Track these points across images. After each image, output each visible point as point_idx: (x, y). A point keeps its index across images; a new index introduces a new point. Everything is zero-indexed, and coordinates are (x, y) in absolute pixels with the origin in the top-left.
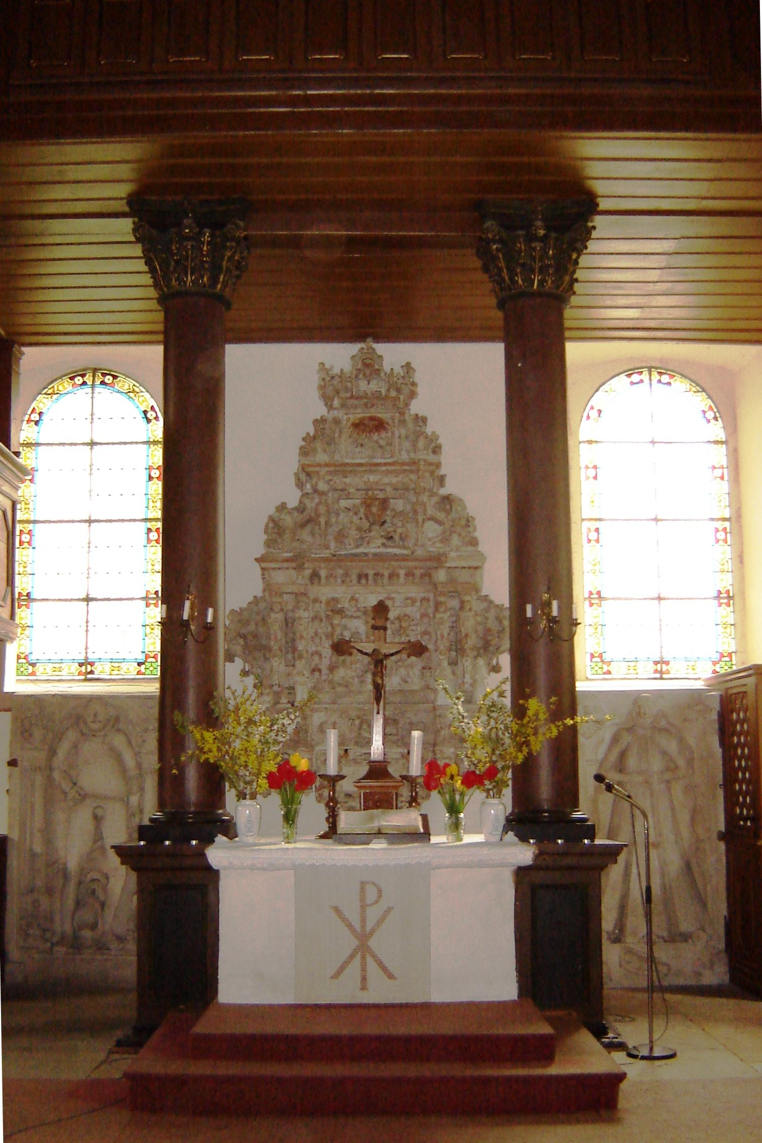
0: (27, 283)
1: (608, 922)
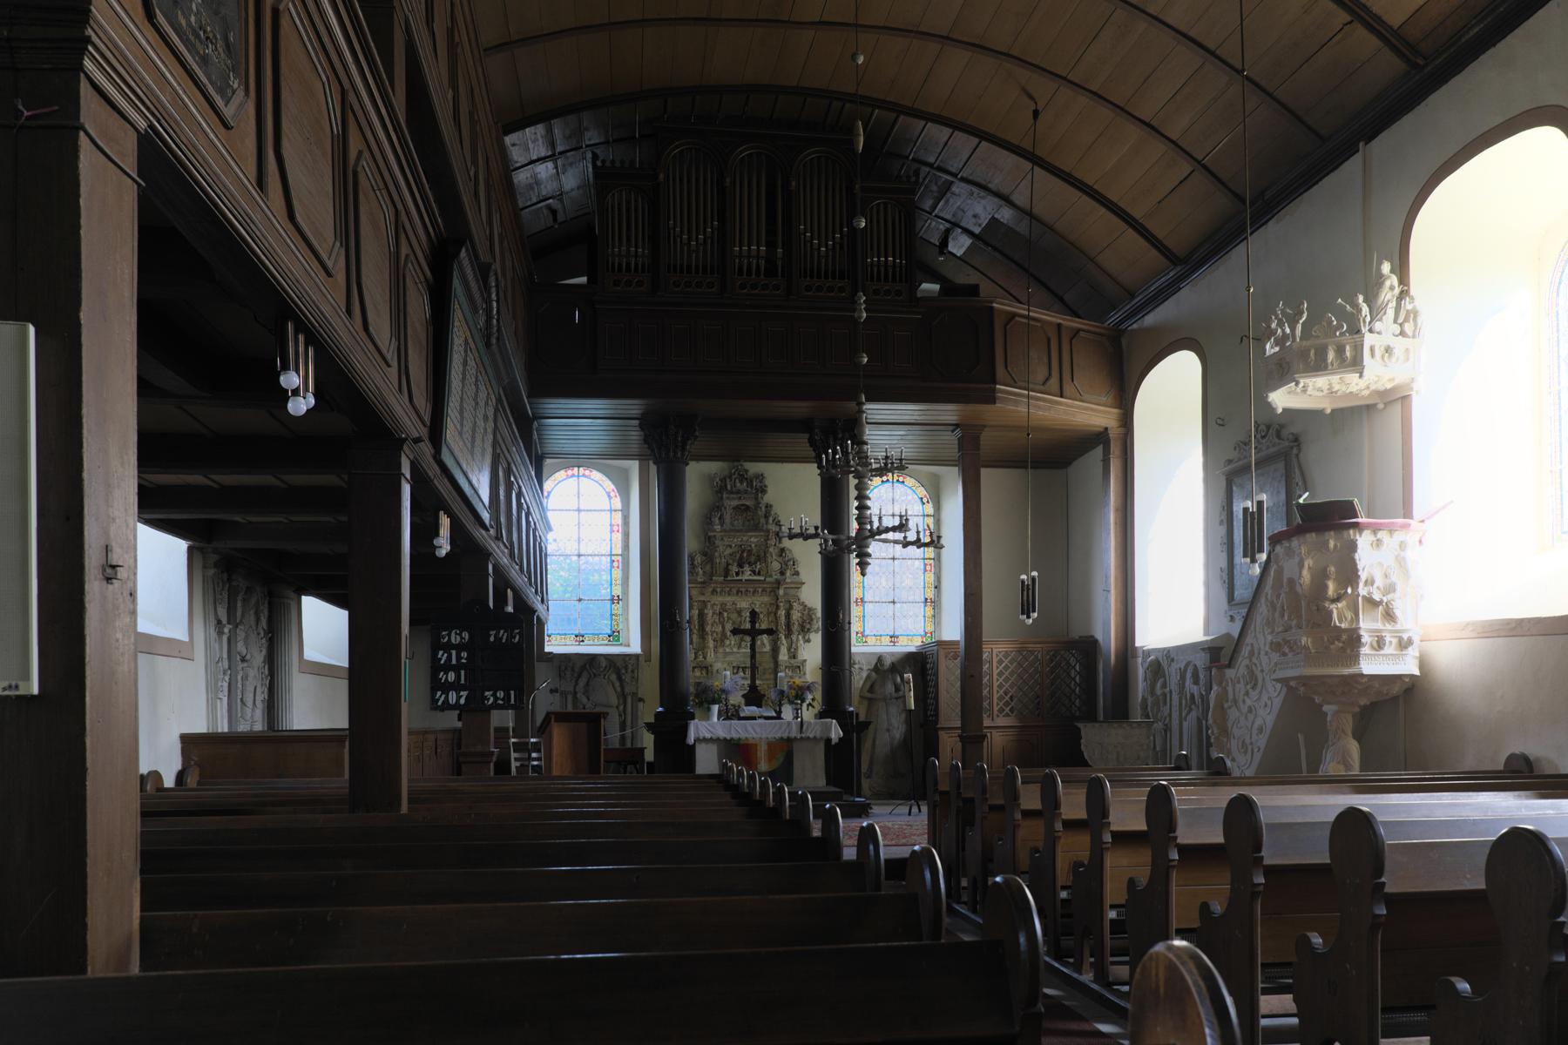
0: (545, 437)
1: (864, 767)
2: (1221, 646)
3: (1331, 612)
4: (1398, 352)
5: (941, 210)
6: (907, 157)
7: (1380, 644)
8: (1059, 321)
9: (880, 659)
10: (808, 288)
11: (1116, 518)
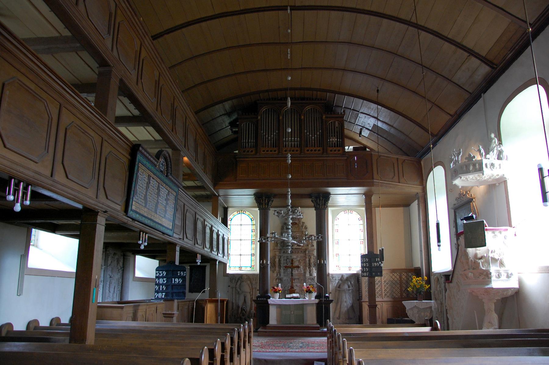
2: (449, 274)
3: (479, 263)
4: (496, 165)
5: (357, 123)
6: (342, 107)
7: (499, 276)
8: (397, 157)
9: (342, 276)
10: (308, 151)
11: (423, 225)
